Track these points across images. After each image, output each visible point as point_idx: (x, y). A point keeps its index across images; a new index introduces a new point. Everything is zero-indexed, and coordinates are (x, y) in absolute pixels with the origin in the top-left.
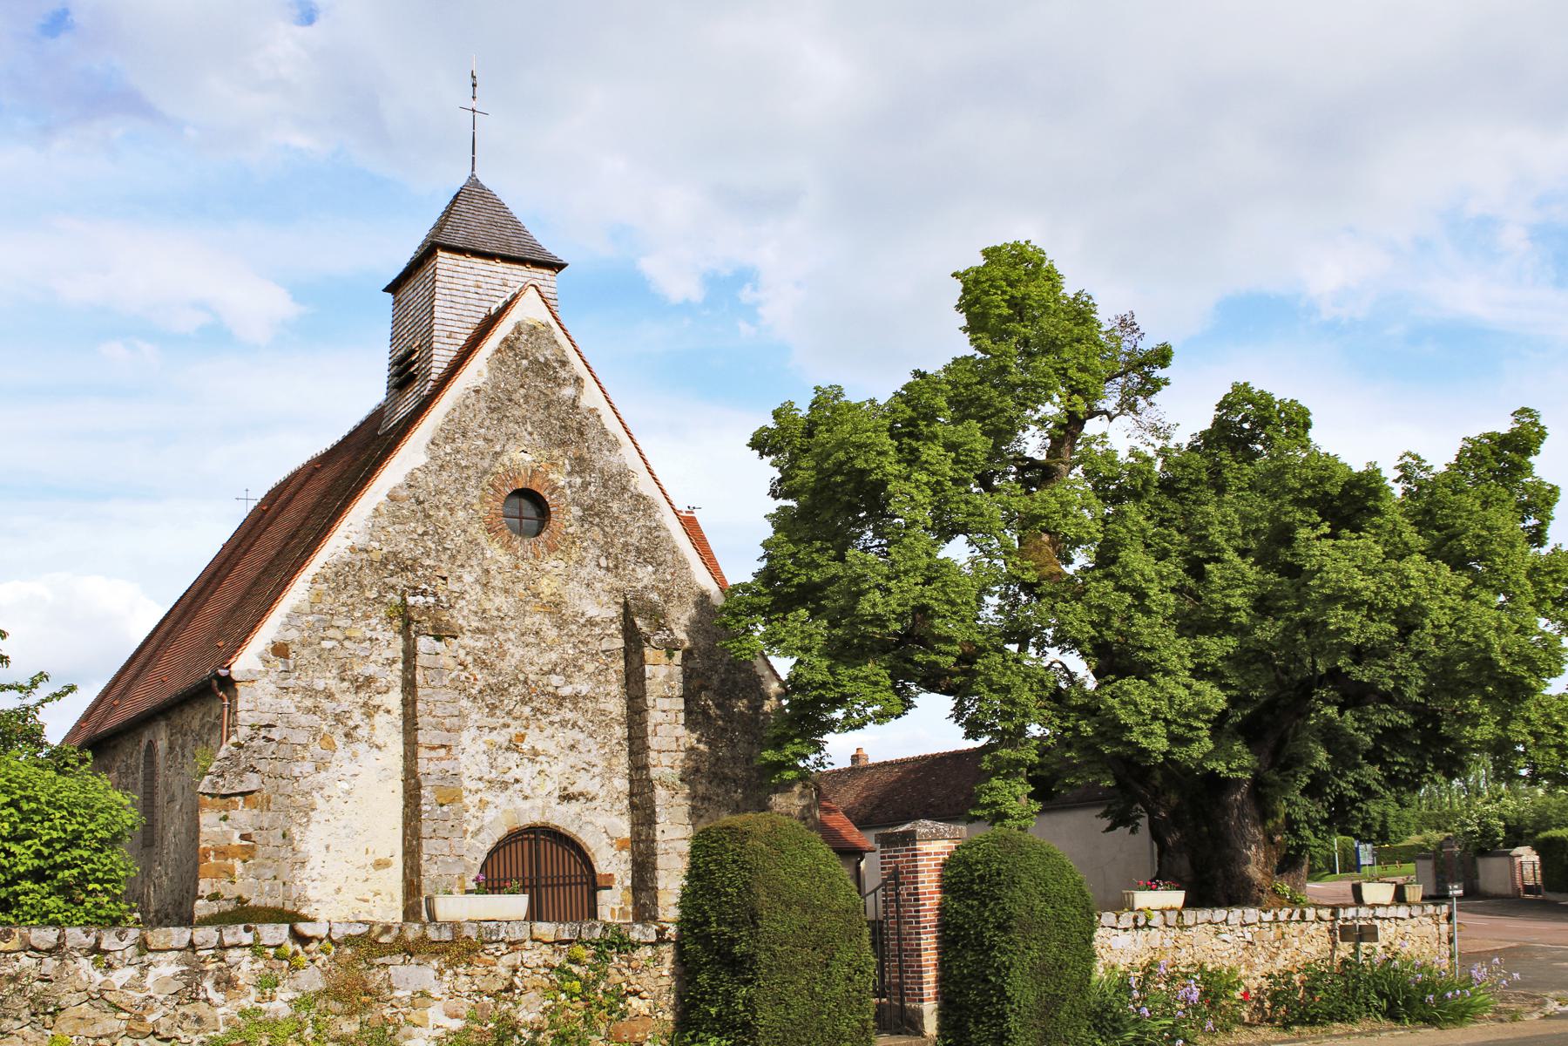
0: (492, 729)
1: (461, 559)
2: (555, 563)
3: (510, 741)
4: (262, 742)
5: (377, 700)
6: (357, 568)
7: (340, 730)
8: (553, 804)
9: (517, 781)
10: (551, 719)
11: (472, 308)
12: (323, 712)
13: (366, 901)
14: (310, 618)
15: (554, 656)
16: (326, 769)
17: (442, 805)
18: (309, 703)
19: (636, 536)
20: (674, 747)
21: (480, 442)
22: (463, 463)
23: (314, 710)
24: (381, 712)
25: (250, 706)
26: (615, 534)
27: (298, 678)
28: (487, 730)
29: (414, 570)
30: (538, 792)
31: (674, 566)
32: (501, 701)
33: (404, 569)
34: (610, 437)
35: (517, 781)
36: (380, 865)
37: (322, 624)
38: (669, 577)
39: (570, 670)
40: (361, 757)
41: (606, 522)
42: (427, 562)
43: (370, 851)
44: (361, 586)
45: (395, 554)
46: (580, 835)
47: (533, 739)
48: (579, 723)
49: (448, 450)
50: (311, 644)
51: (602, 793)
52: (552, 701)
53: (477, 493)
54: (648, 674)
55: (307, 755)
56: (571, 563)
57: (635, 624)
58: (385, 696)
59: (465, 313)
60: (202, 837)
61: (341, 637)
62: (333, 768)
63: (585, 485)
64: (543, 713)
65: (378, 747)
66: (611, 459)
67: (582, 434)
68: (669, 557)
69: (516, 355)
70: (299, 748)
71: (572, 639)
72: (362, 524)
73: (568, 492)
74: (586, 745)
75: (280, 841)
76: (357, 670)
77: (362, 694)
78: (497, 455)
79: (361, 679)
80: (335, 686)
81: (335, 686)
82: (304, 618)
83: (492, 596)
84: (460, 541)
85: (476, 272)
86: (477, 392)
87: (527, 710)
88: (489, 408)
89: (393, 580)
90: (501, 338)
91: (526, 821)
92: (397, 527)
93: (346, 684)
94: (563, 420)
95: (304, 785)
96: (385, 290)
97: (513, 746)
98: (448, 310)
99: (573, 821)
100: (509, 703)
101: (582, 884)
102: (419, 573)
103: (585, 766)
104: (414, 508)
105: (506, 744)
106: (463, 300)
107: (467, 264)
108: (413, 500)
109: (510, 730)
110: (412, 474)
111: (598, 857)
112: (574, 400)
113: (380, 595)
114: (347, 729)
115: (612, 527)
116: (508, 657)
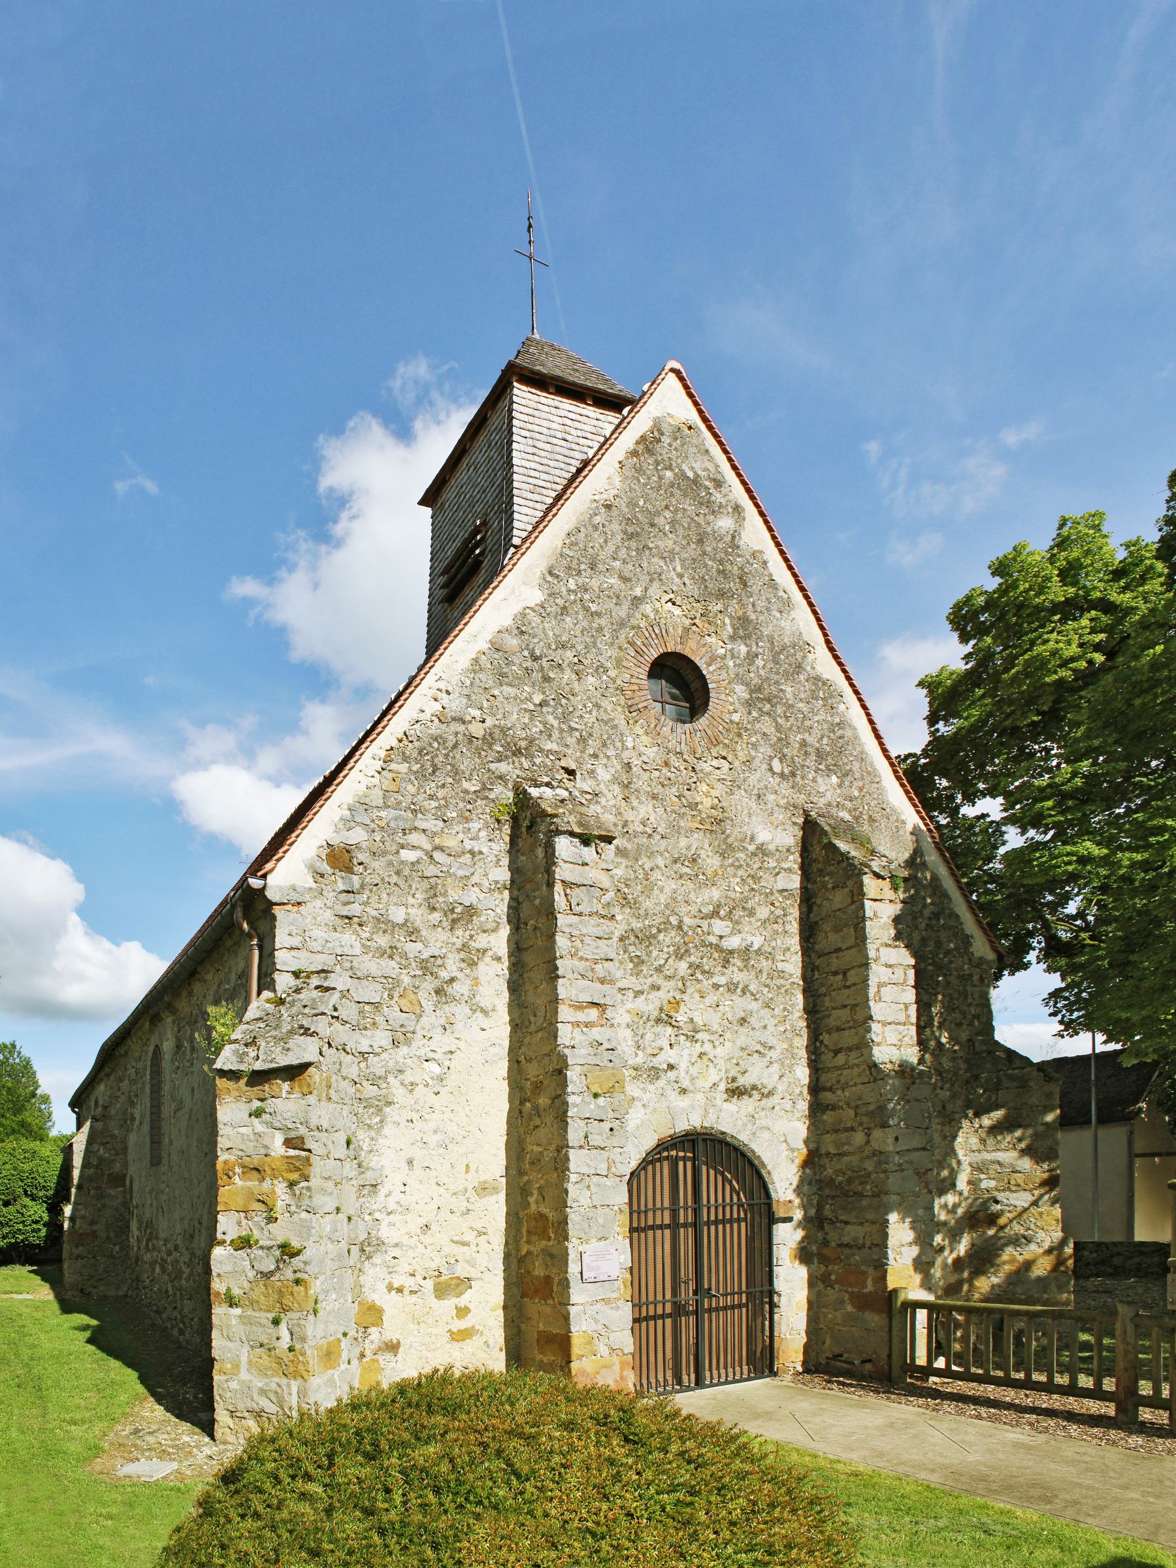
0: (638, 993)
1: (593, 745)
2: (715, 763)
3: (661, 1009)
4: (316, 994)
5: (482, 941)
6: (450, 744)
7: (429, 985)
8: (719, 1102)
9: (671, 1067)
10: (715, 980)
11: (561, 458)
12: (405, 956)
13: (465, 1244)
14: (383, 814)
15: (716, 894)
16: (408, 1042)
17: (596, 1096)
18: (383, 941)
19: (817, 733)
20: (902, 1018)
21: (614, 580)
22: (594, 608)
23: (391, 952)
24: (487, 959)
25: (296, 941)
26: (790, 729)
27: (366, 904)
28: (630, 994)
29: (530, 757)
30: (700, 1083)
31: (863, 779)
32: (649, 954)
33: (518, 752)
34: (781, 593)
35: (671, 1067)
36: (484, 1189)
37: (402, 825)
38: (856, 793)
39: (738, 913)
40: (459, 1026)
41: (780, 710)
42: (549, 746)
43: (473, 1168)
44: (456, 773)
45: (504, 730)
46: (754, 1146)
47: (694, 1010)
48: (752, 988)
49: (572, 585)
50: (384, 853)
51: (781, 1088)
52: (716, 955)
53: (613, 652)
54: (868, 913)
55: (380, 1019)
56: (737, 764)
57: (835, 849)
58: (493, 935)
59: (552, 463)
60: (222, 1142)
61: (429, 847)
62: (418, 1041)
63: (752, 657)
64: (704, 972)
65: (484, 1012)
66: (783, 623)
67: (745, 585)
68: (856, 766)
69: (657, 463)
70: (367, 1008)
71: (740, 873)
72: (455, 680)
73: (731, 664)
74: (760, 1019)
75: (341, 1152)
76: (454, 895)
77: (460, 932)
78: (637, 601)
79: (459, 910)
80: (418, 915)
81: (418, 915)
82: (376, 813)
83: (635, 803)
84: (590, 719)
85: (563, 413)
86: (608, 507)
87: (683, 967)
88: (625, 532)
89: (503, 767)
90: (637, 435)
91: (682, 1126)
92: (507, 690)
93: (436, 916)
94: (721, 562)
95: (376, 1065)
96: (420, 503)
97: (665, 1018)
98: (530, 457)
99: (745, 1125)
100: (657, 957)
101: (739, 1220)
102: (538, 761)
103: (759, 1048)
104: (529, 664)
105: (656, 1013)
106: (548, 447)
107: (550, 402)
108: (526, 653)
109: (661, 993)
110: (524, 615)
111: (776, 1176)
112: (733, 537)
113: (484, 788)
114: (437, 983)
115: (787, 718)
116: (656, 892)
